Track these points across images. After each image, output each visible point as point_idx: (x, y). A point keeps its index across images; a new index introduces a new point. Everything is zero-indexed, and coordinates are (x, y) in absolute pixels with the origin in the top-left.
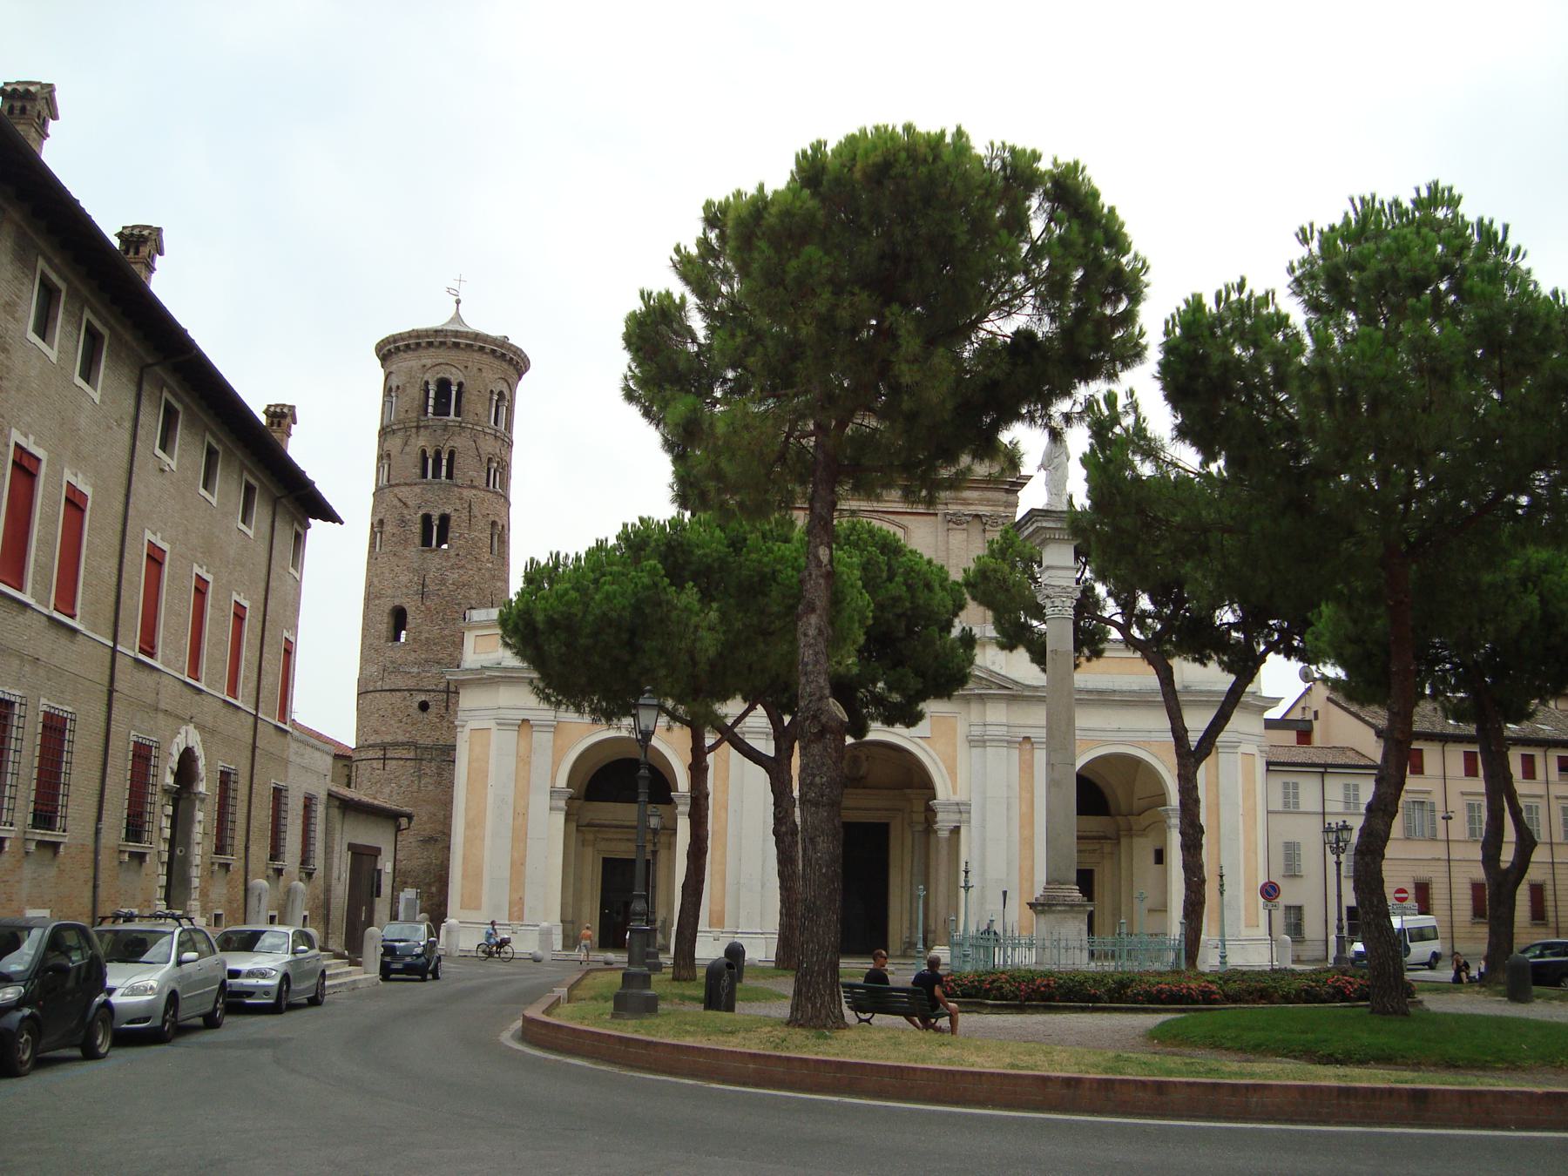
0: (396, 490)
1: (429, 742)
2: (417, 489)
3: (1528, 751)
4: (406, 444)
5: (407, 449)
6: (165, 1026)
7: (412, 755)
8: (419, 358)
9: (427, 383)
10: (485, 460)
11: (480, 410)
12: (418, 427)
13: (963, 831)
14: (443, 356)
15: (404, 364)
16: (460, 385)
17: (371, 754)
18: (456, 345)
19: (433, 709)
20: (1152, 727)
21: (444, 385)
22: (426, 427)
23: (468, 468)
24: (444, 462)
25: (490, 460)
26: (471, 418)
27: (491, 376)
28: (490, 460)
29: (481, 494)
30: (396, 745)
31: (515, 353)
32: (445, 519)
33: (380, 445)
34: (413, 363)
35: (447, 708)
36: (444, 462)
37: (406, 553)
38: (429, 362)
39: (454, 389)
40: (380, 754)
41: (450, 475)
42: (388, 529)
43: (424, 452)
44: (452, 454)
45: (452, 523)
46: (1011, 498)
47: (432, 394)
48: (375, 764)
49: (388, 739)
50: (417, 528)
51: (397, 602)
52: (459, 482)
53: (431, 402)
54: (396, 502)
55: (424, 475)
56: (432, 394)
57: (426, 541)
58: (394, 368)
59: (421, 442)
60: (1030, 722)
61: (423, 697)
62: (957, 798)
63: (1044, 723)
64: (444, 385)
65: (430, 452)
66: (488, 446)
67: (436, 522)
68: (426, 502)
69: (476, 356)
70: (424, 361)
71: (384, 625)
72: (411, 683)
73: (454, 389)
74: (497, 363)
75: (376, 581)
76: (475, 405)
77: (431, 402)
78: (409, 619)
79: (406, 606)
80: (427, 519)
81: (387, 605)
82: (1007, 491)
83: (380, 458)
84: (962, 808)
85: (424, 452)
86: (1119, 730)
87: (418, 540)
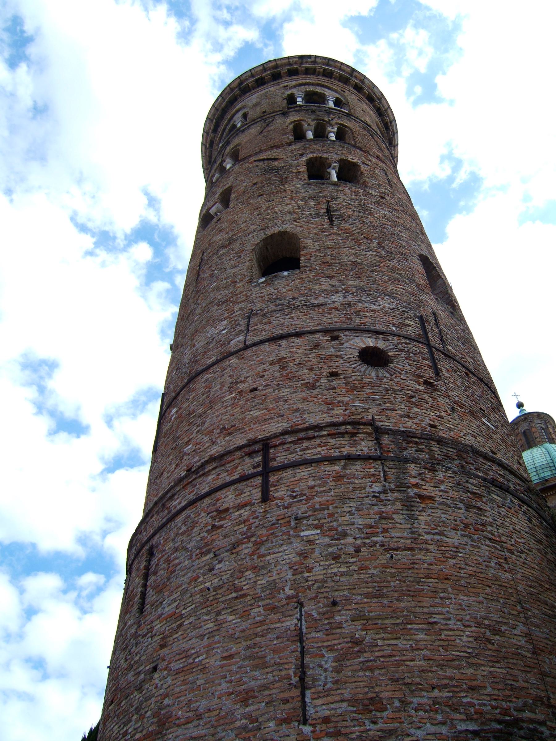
7: (366, 446)
71: (242, 265)
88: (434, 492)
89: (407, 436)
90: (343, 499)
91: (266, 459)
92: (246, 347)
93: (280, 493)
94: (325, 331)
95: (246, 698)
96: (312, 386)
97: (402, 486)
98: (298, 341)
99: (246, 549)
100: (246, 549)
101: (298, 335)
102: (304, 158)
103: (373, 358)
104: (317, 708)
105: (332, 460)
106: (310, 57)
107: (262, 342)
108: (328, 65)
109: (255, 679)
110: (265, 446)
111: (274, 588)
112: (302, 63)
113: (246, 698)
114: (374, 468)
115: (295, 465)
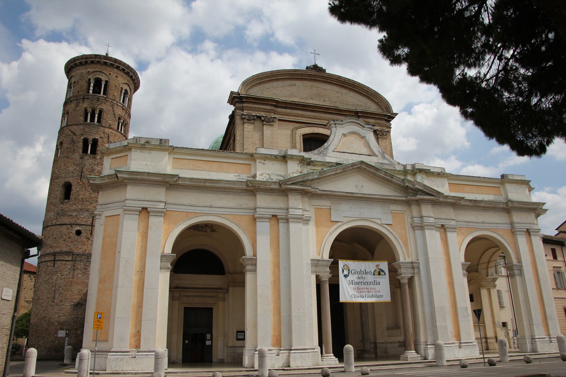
0: (70, 127)
1: (80, 251)
2: (81, 127)
3: (554, 247)
4: (77, 106)
5: (78, 108)
6: (493, 77)
7: (70, 258)
8: (86, 68)
9: (90, 79)
10: (117, 117)
11: (116, 94)
12: (84, 99)
13: (416, 279)
14: (98, 68)
15: (78, 72)
16: (107, 82)
17: (47, 258)
18: (106, 64)
19: (84, 234)
20: (498, 221)
21: (98, 82)
22: (88, 99)
23: (108, 119)
24: (97, 115)
25: (119, 118)
26: (111, 97)
27: (120, 81)
28: (119, 118)
29: (115, 132)
30: (61, 253)
31: (134, 74)
32: (95, 142)
33: (64, 109)
34: (84, 71)
35: (91, 234)
36: (97, 115)
37: (74, 156)
38: (91, 70)
39: (103, 83)
40: (52, 258)
41: (99, 121)
42: (65, 145)
43: (86, 110)
44: (101, 112)
45: (99, 143)
46: (388, 124)
47: (92, 85)
48: (49, 264)
49: (58, 250)
50: (81, 145)
51: (67, 180)
52: (104, 125)
53: (91, 88)
54: (70, 133)
55: (86, 120)
56: (92, 85)
57: (85, 151)
58: (73, 74)
59: (85, 105)
60: (443, 217)
61: (78, 228)
62: (409, 260)
63: (116, 319)
64: (98, 82)
65: (89, 110)
66: (119, 112)
67: (97, 112)
68: (85, 132)
69: (115, 70)
70: (89, 70)
71: (60, 192)
72: (72, 221)
73: (103, 83)
74: (125, 76)
75: (56, 171)
76: (114, 93)
77: (91, 88)
78: (73, 188)
79: (72, 182)
80: (86, 141)
81: (62, 181)
82: (386, 120)
83: (63, 115)
84: (414, 266)
85: (86, 110)
86: (483, 223)
87: (81, 151)
88: (79, 267)
89: (78, 255)
90: (64, 269)
91: (55, 258)
92: (56, 225)
93: (56, 266)
94: (71, 224)
95: (48, 298)
96: (65, 241)
97: (74, 266)
98: (65, 226)
99: (50, 275)
100: (50, 275)
101: (65, 224)
102: (82, 138)
103: (79, 233)
104: (55, 301)
105: (64, 260)
106: (98, 55)
107: (58, 225)
108: (106, 59)
109: (49, 296)
110: (55, 254)
111: (53, 283)
112: (96, 58)
113: (48, 298)
114: (71, 263)
115: (59, 260)
